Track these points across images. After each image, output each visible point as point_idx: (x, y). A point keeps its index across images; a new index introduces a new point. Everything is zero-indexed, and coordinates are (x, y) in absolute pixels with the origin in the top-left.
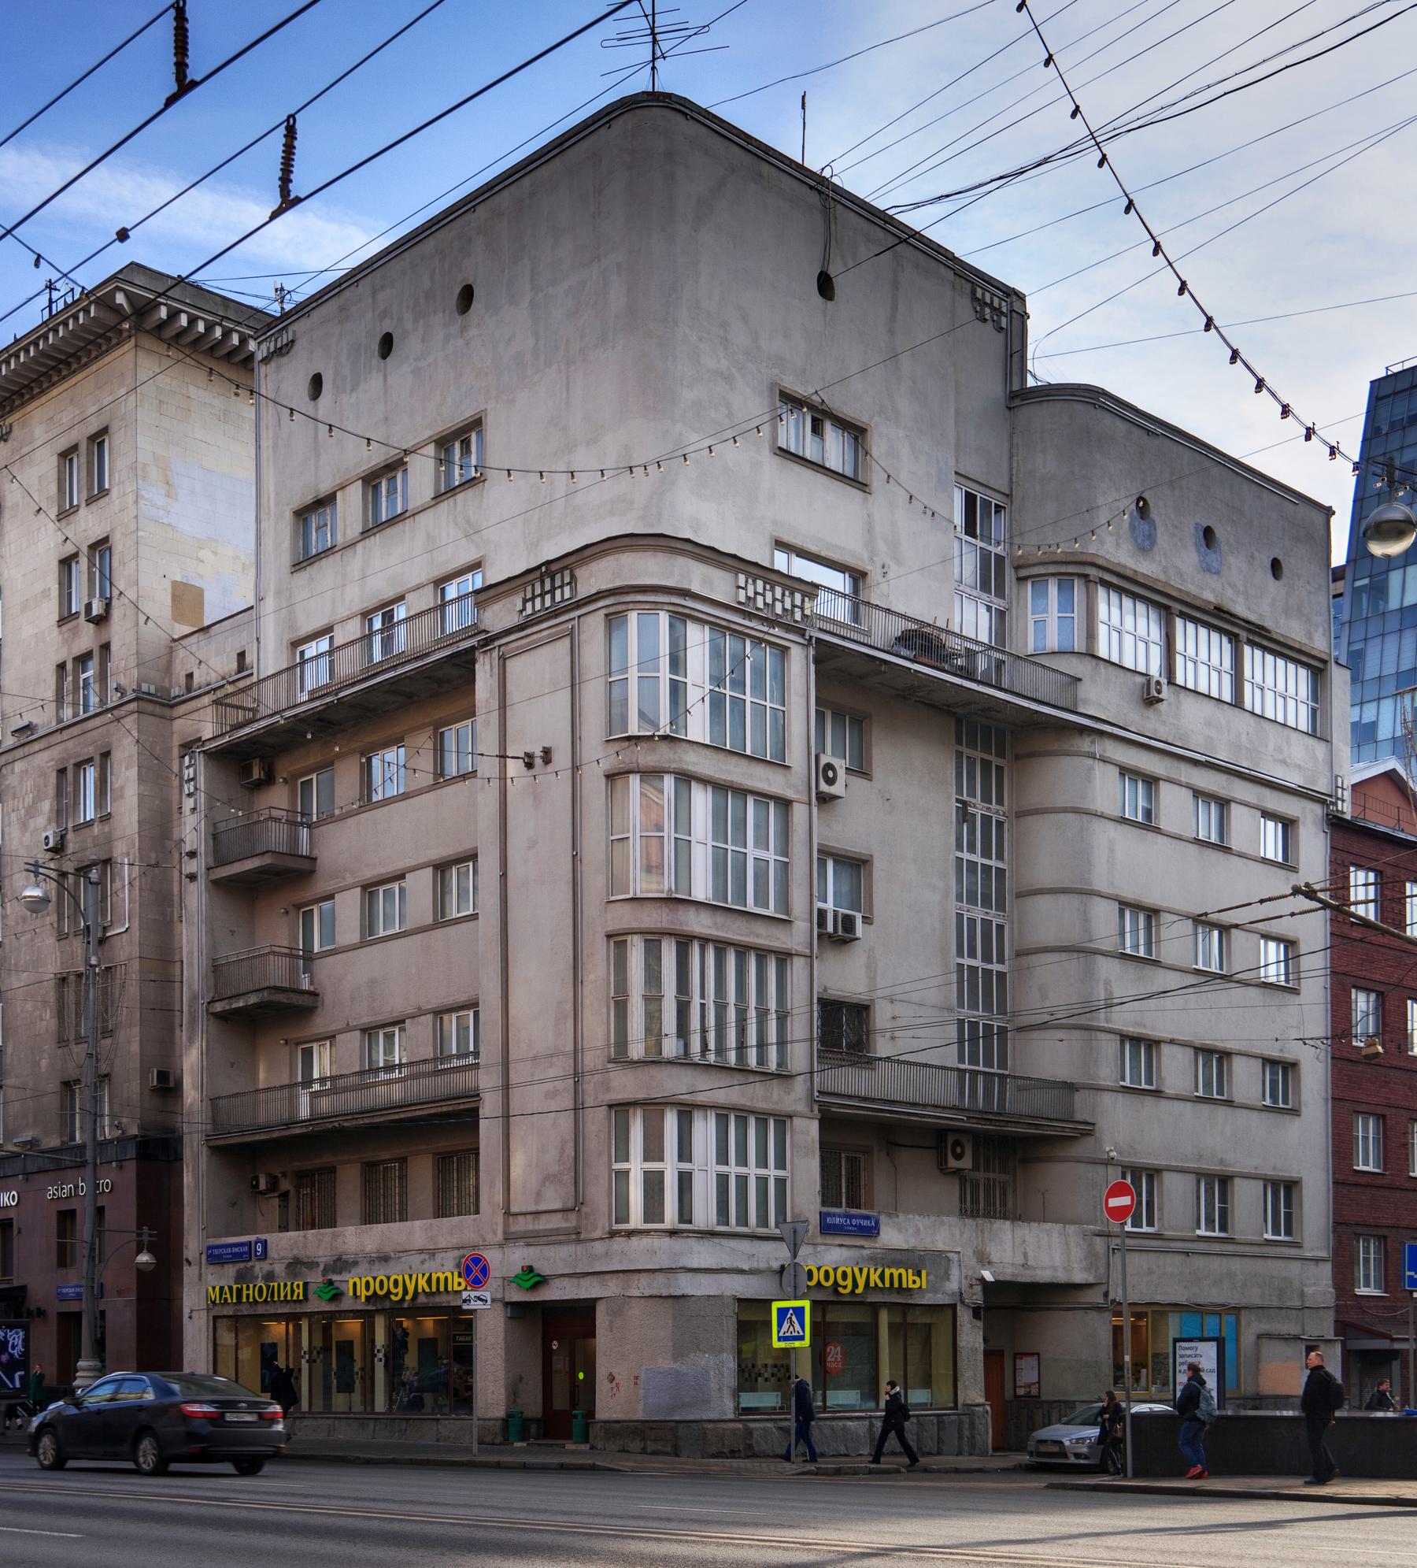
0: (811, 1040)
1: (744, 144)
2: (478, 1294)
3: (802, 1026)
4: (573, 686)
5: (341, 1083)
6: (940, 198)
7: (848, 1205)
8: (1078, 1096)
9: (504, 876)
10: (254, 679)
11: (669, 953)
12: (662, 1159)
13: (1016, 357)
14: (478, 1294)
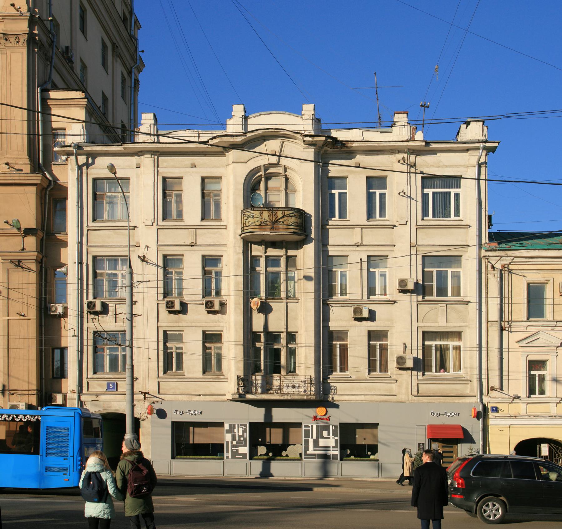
1: (132, 102)
5: (344, 278)
6: (385, 287)
7: (449, 193)
8: (462, 180)
9: (487, 341)
12: (437, 296)
13: (133, 122)
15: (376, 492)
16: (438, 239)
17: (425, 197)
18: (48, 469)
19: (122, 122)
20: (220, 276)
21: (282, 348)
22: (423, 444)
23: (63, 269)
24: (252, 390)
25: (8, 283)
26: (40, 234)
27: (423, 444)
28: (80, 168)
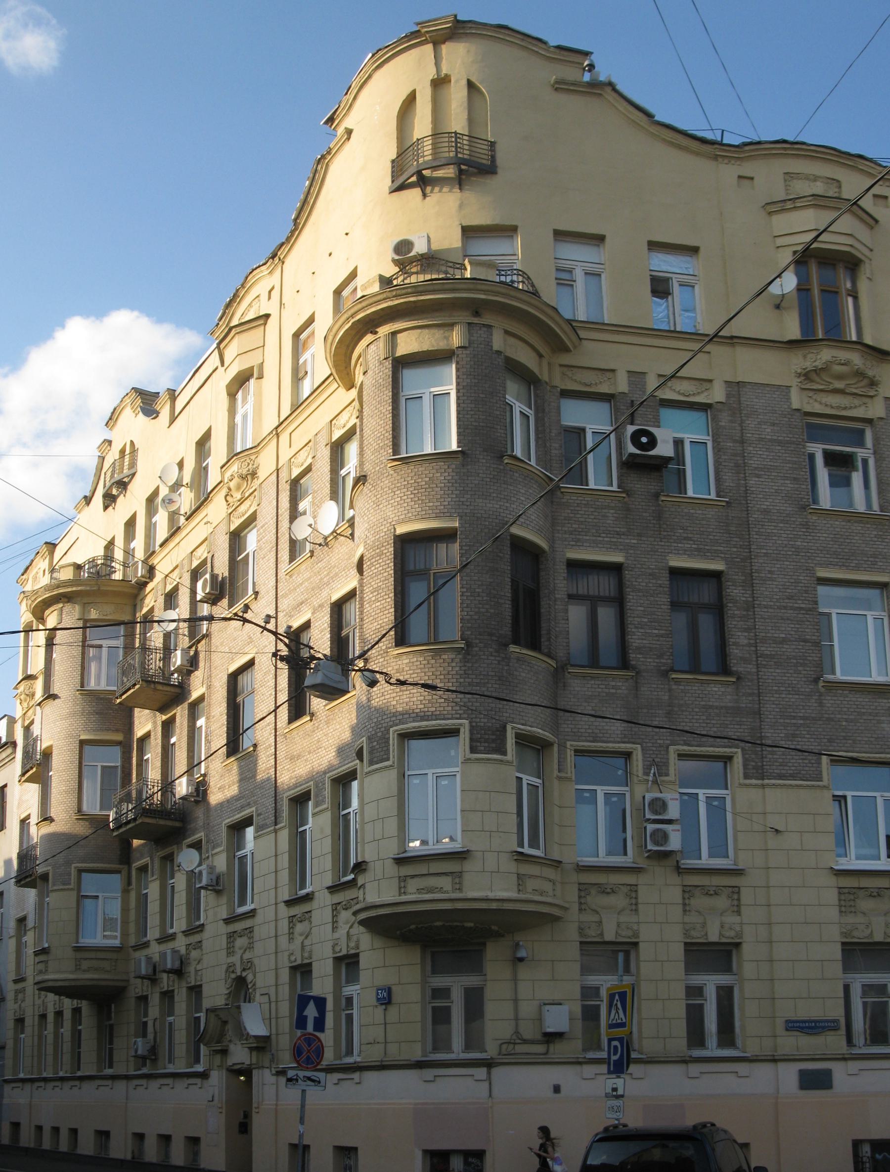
2: (309, 1074)
14: (309, 1074)
16: (231, 960)
20: (203, 1079)
22: (194, 1141)
23: (397, 257)
25: (277, 1100)
26: (725, 419)
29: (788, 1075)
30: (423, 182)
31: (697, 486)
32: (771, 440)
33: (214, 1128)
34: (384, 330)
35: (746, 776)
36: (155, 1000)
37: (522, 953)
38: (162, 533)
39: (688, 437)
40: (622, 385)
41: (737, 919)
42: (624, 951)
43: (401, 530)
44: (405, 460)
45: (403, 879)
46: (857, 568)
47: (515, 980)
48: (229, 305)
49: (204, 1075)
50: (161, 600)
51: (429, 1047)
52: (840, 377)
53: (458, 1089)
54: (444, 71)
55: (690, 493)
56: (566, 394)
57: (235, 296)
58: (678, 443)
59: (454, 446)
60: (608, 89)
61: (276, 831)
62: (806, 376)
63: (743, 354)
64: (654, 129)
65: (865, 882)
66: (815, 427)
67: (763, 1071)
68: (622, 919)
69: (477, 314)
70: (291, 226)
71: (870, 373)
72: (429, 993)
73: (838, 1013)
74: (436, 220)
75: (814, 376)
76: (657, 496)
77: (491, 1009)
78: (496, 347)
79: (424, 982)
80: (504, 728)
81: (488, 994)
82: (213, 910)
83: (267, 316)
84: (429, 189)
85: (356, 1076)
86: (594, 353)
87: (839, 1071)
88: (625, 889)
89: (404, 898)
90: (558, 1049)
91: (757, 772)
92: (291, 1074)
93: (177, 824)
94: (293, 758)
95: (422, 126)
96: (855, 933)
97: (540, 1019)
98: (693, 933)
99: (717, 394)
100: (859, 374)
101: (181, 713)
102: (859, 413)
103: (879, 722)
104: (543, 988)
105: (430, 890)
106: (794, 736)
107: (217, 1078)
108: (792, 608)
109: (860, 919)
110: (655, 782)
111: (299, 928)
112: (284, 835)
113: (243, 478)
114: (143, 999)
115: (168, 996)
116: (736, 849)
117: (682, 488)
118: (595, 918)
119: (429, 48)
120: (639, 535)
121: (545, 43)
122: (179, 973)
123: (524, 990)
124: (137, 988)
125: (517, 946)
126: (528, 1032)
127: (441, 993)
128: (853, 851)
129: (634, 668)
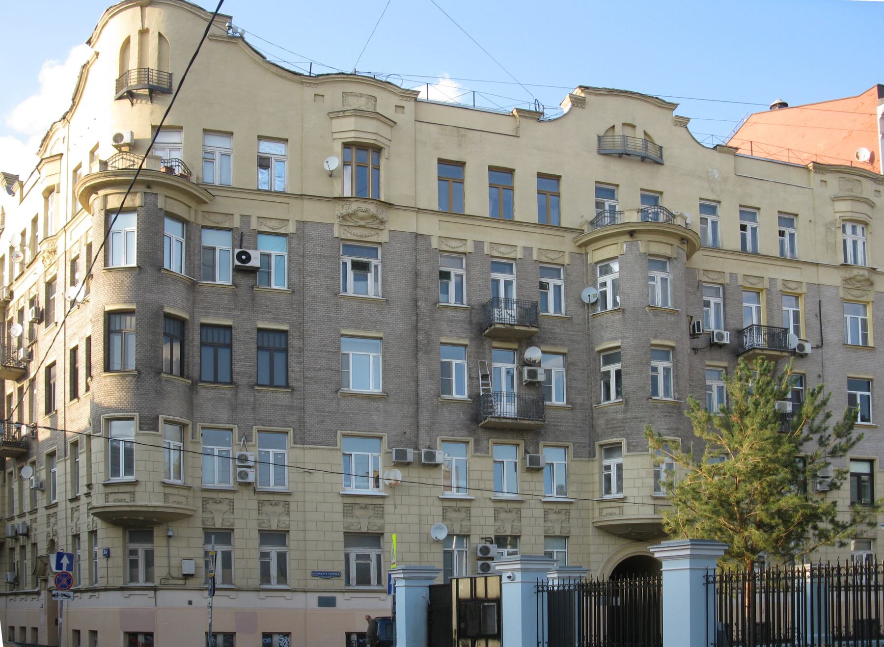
0: (304, 448)
2: (64, 592)
3: (50, 450)
4: (306, 592)
10: (643, 245)
11: (850, 261)
14: (64, 592)
15: (150, 49)
17: (347, 556)
18: (586, 244)
19: (830, 394)
21: (658, 552)
22: (35, 630)
24: (693, 433)
26: (295, 242)
27: (35, 630)
28: (108, 213)
29: (312, 599)
30: (131, 95)
31: (278, 283)
32: (320, 256)
33: (42, 621)
34: (102, 193)
35: (295, 443)
36: (18, 550)
37: (170, 533)
38: (17, 273)
39: (274, 253)
40: (236, 223)
41: (287, 518)
42: (225, 535)
43: (108, 308)
44: (110, 270)
45: (107, 494)
46: (365, 329)
47: (168, 546)
48: (44, 140)
49: (38, 593)
50: (28, 303)
51: (128, 579)
52: (362, 219)
53: (140, 601)
54: (146, 26)
55: (273, 286)
56: (204, 227)
57: (47, 135)
58: (266, 257)
59: (135, 265)
60: (240, 41)
61: (65, 460)
62: (343, 217)
63: (308, 205)
64: (266, 65)
65: (358, 501)
66: (350, 247)
67: (300, 597)
68: (225, 516)
69: (149, 187)
70: (71, 103)
71: (380, 216)
72: (127, 552)
73: (341, 568)
74: (138, 120)
75: (347, 218)
76: (252, 287)
77: (157, 561)
78: (159, 206)
79: (124, 547)
80: (158, 417)
81: (156, 554)
82: (42, 501)
83: (62, 154)
84: (135, 100)
85: (96, 594)
86: (223, 204)
87: (339, 598)
88: (227, 501)
89: (107, 504)
90: (191, 583)
91: (301, 440)
92: (54, 592)
93: (24, 450)
94: (72, 421)
95: (133, 64)
96: (352, 527)
97: (180, 567)
98: (263, 525)
99: (291, 228)
100: (374, 217)
101: (26, 383)
102: (374, 239)
103: (371, 415)
104: (182, 551)
105: (120, 501)
106: (322, 422)
107: (44, 594)
108: (326, 351)
109: (354, 520)
110: (244, 445)
111: (76, 514)
112: (69, 462)
113: (50, 253)
114: (12, 549)
115: (23, 547)
116: (289, 482)
117: (269, 284)
118: (211, 516)
119: (139, 8)
120: (241, 310)
121: (204, 10)
122: (27, 535)
123: (173, 552)
124: (9, 543)
125: (168, 530)
126: (175, 573)
127: (134, 552)
128: (353, 484)
129: (235, 383)
